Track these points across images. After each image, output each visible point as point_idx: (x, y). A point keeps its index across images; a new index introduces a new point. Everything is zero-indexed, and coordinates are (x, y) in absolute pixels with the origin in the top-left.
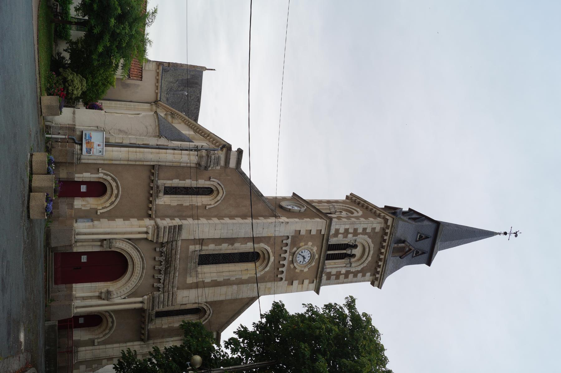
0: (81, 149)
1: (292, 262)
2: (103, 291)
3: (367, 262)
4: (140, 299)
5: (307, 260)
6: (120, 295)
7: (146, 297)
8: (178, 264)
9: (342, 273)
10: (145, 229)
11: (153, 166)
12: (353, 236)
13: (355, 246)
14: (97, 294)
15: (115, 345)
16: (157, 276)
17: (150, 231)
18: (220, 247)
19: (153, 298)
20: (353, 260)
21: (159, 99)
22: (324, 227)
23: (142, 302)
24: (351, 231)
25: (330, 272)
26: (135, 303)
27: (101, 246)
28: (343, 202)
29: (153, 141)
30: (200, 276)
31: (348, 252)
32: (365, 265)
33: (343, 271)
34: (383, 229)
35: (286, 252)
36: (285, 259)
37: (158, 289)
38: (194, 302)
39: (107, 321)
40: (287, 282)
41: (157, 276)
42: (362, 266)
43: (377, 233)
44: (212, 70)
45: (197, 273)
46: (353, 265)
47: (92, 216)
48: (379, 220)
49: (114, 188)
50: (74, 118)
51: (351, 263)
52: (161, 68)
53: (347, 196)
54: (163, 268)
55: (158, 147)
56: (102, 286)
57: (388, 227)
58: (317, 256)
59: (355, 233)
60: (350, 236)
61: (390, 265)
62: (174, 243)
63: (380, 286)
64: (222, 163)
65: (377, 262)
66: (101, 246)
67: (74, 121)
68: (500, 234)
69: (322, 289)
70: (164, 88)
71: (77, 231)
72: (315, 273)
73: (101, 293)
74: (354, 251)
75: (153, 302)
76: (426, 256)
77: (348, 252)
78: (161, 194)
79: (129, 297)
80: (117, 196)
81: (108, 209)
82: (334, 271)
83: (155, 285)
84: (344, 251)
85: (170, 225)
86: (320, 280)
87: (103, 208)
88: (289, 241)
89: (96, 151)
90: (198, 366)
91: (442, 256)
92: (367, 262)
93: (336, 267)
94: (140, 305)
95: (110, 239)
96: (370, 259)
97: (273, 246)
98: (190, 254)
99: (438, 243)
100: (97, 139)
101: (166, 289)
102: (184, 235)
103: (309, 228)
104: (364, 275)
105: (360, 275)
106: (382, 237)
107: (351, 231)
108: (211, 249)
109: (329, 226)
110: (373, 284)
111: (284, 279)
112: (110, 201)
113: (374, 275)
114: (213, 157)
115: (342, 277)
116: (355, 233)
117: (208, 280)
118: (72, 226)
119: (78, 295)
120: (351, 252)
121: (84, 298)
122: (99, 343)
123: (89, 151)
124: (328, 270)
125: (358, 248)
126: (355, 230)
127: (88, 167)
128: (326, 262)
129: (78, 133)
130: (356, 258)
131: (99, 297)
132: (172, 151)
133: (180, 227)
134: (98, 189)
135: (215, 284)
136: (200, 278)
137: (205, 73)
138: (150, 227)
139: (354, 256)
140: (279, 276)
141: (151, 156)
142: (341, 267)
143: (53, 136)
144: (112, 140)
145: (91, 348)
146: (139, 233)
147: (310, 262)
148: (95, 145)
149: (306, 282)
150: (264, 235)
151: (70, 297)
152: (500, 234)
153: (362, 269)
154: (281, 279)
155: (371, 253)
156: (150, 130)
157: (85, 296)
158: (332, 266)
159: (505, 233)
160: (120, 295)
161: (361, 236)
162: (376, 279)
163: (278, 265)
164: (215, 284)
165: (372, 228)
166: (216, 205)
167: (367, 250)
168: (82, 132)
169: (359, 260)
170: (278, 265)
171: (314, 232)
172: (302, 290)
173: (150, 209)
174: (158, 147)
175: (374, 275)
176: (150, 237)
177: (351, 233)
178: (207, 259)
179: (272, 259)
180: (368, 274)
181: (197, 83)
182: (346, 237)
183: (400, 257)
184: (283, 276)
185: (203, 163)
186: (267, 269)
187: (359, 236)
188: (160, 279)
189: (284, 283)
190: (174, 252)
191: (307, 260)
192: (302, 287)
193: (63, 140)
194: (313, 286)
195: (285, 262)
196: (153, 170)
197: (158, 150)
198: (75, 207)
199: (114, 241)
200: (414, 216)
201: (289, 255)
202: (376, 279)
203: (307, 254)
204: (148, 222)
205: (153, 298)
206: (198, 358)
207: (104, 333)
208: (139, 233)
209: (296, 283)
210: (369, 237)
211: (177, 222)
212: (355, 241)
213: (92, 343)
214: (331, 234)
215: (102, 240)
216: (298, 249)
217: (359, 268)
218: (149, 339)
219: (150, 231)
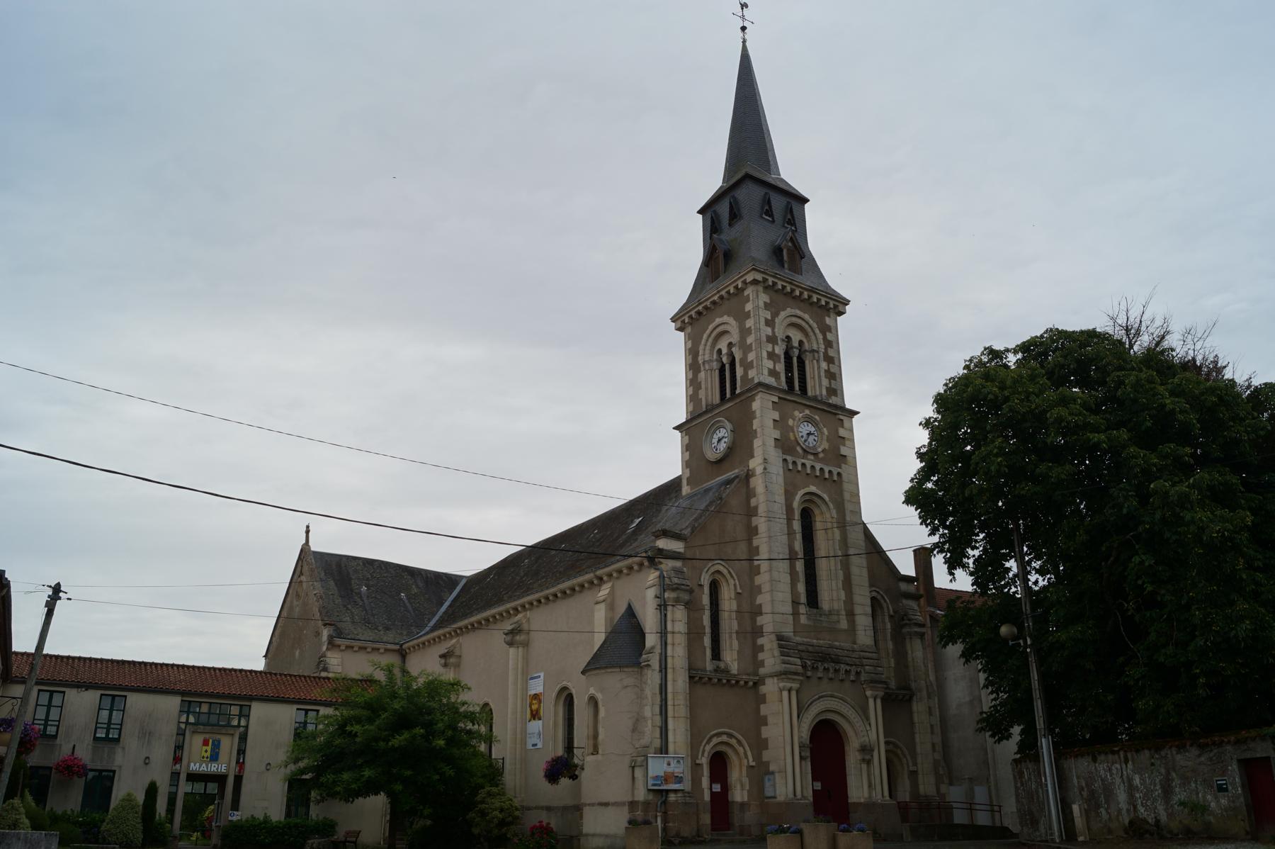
0: (676, 791)
1: (815, 454)
2: (859, 757)
3: (811, 322)
4: (871, 701)
5: (813, 429)
6: (865, 730)
7: (869, 693)
8: (823, 642)
10: (785, 694)
11: (691, 678)
14: (864, 766)
15: (918, 740)
16: (842, 675)
19: (872, 681)
20: (807, 346)
21: (397, 647)
22: (768, 397)
26: (875, 708)
29: (653, 678)
30: (836, 607)
32: (815, 325)
33: (824, 365)
34: (766, 288)
35: (803, 465)
36: (813, 467)
37: (858, 674)
38: (870, 619)
41: (842, 675)
42: (817, 331)
43: (771, 299)
44: (308, 532)
45: (830, 613)
46: (815, 347)
47: (760, 772)
48: (749, 291)
49: (720, 739)
50: (616, 804)
51: (813, 351)
52: (338, 641)
53: (678, 329)
54: (831, 666)
55: (664, 669)
56: (852, 758)
57: (765, 280)
58: (807, 412)
59: (772, 340)
61: (806, 280)
62: (800, 647)
63: (846, 302)
64: (678, 564)
65: (812, 304)
67: (623, 804)
68: (744, 42)
69: (848, 406)
70: (369, 635)
71: (791, 795)
73: (863, 760)
75: (876, 682)
76: (795, 206)
78: (722, 665)
79: (868, 719)
81: (747, 748)
82: (825, 382)
83: (852, 678)
84: (795, 360)
85: (776, 653)
86: (836, 407)
88: (789, 458)
89: (676, 769)
90: (1015, 630)
92: (811, 322)
94: (879, 702)
96: (806, 317)
98: (810, 623)
99: (771, 179)
100: (657, 767)
101: (857, 661)
102: (788, 630)
103: (771, 423)
105: (829, 336)
106: (777, 291)
109: (768, 387)
110: (841, 313)
112: (736, 746)
113: (828, 310)
114: (676, 580)
116: (772, 340)
117: (843, 595)
118: (780, 804)
119: (866, 795)
122: (915, 764)
123: (679, 780)
124: (824, 392)
127: (696, 781)
128: (810, 394)
129: (651, 797)
131: (869, 762)
132: (669, 648)
133: (780, 638)
134: (719, 764)
135: (848, 584)
136: (839, 605)
137: (315, 546)
138: (781, 685)
139: (801, 343)
140: (835, 478)
141: (678, 683)
144: (657, 743)
145: (920, 776)
147: (815, 424)
148: (670, 770)
149: (842, 432)
150: (783, 501)
151: (870, 806)
152: (744, 42)
154: (839, 474)
155: (799, 312)
156: (629, 681)
157: (863, 785)
158: (817, 386)
159: (743, 29)
160: (865, 730)
162: (836, 307)
163: (821, 479)
164: (848, 584)
167: (799, 321)
168: (649, 790)
169: (806, 335)
170: (821, 479)
171: (776, 416)
172: (852, 440)
173: (746, 683)
174: (664, 669)
175: (828, 310)
178: (813, 598)
179: (813, 489)
181: (339, 565)
182: (778, 356)
185: (686, 597)
186: (825, 497)
189: (844, 470)
190: (810, 649)
191: (813, 429)
193: (665, 821)
195: (818, 466)
196: (695, 678)
197: (669, 671)
198: (746, 799)
200: (723, 209)
202: (836, 307)
203: (806, 428)
204: (770, 687)
205: (872, 681)
206: (1004, 630)
209: (844, 451)
211: (768, 642)
213: (913, 775)
214: (775, 384)
215: (802, 758)
217: (820, 336)
218: (908, 688)
219: (789, 685)
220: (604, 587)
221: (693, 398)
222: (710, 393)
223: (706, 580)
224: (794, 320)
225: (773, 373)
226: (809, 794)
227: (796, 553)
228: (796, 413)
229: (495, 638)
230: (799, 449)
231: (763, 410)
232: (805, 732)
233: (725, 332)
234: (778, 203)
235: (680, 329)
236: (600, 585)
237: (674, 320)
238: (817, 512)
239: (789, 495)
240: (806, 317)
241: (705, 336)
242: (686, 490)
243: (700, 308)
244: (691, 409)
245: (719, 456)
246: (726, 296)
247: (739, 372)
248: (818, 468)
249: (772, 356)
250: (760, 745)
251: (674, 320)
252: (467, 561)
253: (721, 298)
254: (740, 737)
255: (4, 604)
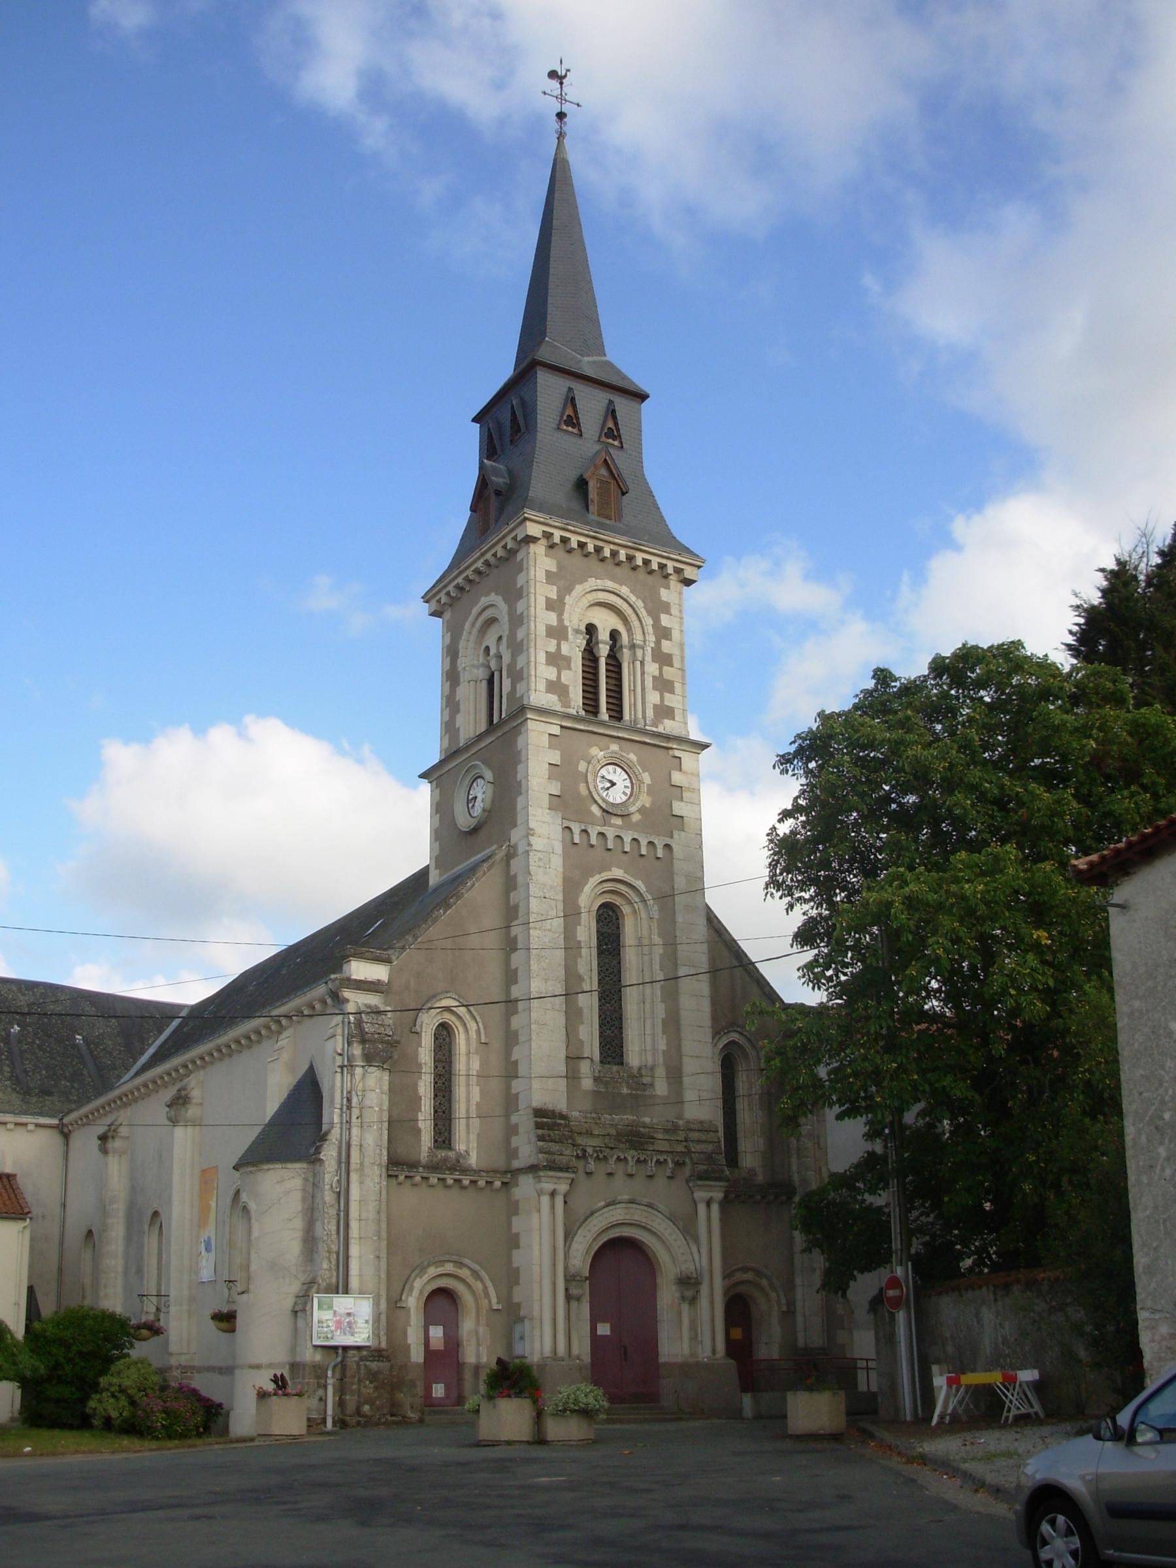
3: (633, 598)
4: (702, 1208)
9: (657, 673)
10: (545, 1200)
12: (566, 639)
13: (591, 629)
14: (685, 1307)
17: (548, 1186)
18: (586, 1012)
21: (55, 1121)
23: (709, 1203)
24: (552, 646)
25: (655, 706)
26: (709, 1219)
27: (578, 1299)
28: (454, 633)
31: (603, 651)
32: (639, 604)
33: (652, 668)
39: (742, 1282)
40: (676, 834)
42: (643, 613)
43: (560, 567)
47: (511, 1316)
56: (667, 1295)
58: (614, 747)
60: (565, 649)
66: (578, 1299)
72: (655, 749)
74: (604, 635)
76: (622, 405)
77: (603, 651)
79: (696, 1240)
80: (460, 1265)
81: (489, 1284)
87: (487, 1295)
91: (624, 350)
92: (633, 598)
93: (643, 689)
94: (715, 1208)
95: (566, 1280)
96: (624, 590)
97: (588, 873)
99: (587, 364)
104: (666, 608)
105: (665, 620)
107: (552, 646)
108: (589, 1033)
111: (668, 841)
112: (471, 1280)
113: (666, 576)
115: (669, 673)
119: (686, 1351)
120: (605, 643)
121: (694, 1338)
124: (650, 713)
125: (596, 622)
126: (551, 632)
128: (626, 716)
130: (621, 628)
131: (693, 1301)
134: (443, 1301)
135: (672, 1023)
139: (614, 635)
140: (644, 851)
142: (643, 673)
143: (330, 1411)
146: (553, 1207)
149: (677, 778)
151: (686, 1369)
152: (561, 136)
153: (649, 613)
155: (609, 584)
158: (641, 699)
159: (561, 116)
161: (566, 616)
164: (672, 1023)
165: (548, 582)
166: (479, 1020)
167: (613, 599)
171: (555, 757)
176: (563, 1187)
177: (559, 646)
178: (612, 1045)
179: (617, 873)
180: (664, 594)
182: (567, 660)
183: (623, 494)
184: (659, 842)
187: (567, 623)
188: (658, 1161)
192: (689, 789)
194: (687, 759)
199: (572, 1270)
201: (611, 826)
207: (767, 1288)
208: (553, 1207)
209: (678, 808)
210: (569, 590)
212: (577, 631)
214: (558, 707)
215: (569, 1298)
216: (596, 802)
217: (648, 621)
220: (285, 1034)
221: (449, 728)
222: (471, 723)
223: (428, 1023)
224: (602, 597)
225: (556, 687)
226: (582, 1348)
227: (580, 979)
228: (595, 751)
229: (155, 1109)
230: (595, 809)
231: (539, 746)
232: (580, 1258)
233: (492, 621)
234: (591, 404)
235: (435, 614)
236: (279, 1033)
237: (427, 598)
238: (626, 909)
239: (571, 886)
240: (624, 590)
241: (467, 626)
242: (434, 879)
243: (460, 580)
244: (446, 745)
245: (473, 823)
246: (492, 561)
247: (507, 684)
248: (627, 839)
249: (555, 659)
250: (511, 1277)
251: (427, 598)
252: (191, 989)
253: (487, 564)
254: (477, 1267)
255: (749, 973)
